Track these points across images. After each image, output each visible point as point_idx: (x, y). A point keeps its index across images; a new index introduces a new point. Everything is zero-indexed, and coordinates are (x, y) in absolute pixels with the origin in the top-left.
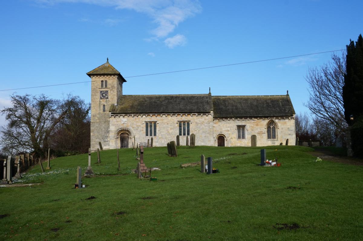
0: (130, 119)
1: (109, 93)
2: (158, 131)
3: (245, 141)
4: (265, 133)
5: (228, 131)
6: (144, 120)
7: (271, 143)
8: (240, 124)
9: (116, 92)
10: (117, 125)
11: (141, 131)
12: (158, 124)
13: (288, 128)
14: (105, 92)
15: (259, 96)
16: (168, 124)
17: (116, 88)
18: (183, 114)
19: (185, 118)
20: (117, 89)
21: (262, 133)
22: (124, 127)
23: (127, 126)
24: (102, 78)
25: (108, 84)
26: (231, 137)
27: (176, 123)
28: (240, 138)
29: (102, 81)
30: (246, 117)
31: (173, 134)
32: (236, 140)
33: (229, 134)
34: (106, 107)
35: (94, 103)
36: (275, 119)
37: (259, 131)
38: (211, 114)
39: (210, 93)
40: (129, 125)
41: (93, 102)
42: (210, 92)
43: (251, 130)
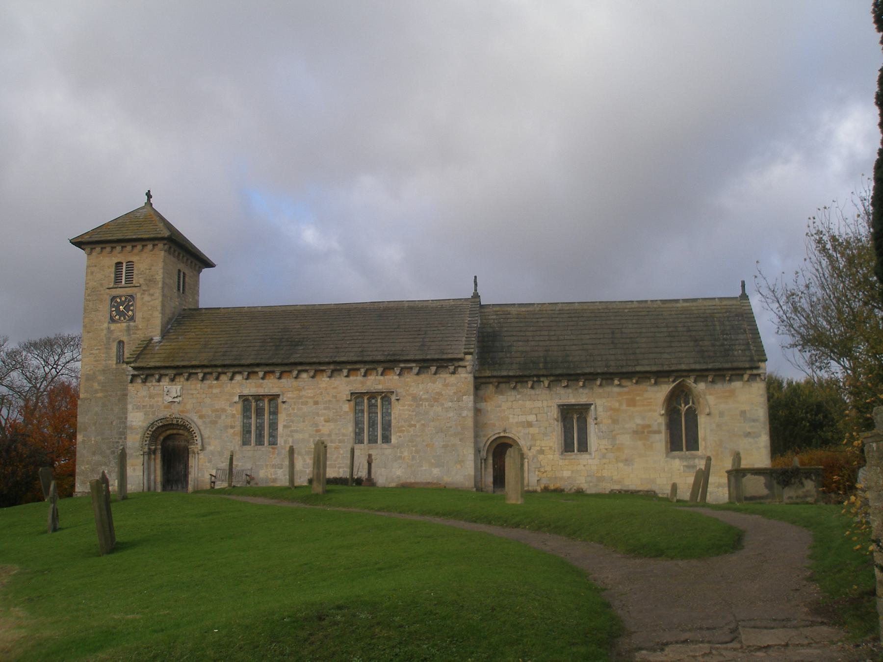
0: (193, 387)
1: (139, 303)
2: (285, 427)
3: (590, 461)
4: (659, 432)
5: (530, 425)
6: (238, 391)
7: (682, 468)
8: (572, 400)
9: (160, 299)
10: (152, 407)
11: (226, 427)
12: (284, 402)
13: (743, 413)
14: (126, 299)
15: (646, 301)
16: (316, 403)
17: (160, 285)
18: (367, 367)
19: (375, 382)
20: (163, 288)
21: (649, 432)
22: (175, 412)
23: (183, 412)
24: (119, 256)
25: (135, 272)
26: (538, 448)
27: (345, 398)
28: (376, 442)
29: (119, 264)
30: (590, 378)
31: (333, 437)
32: (557, 456)
33: (533, 435)
34: (126, 346)
35: (90, 334)
36: (695, 382)
37: (638, 425)
38: (465, 367)
39: (476, 296)
40: (189, 406)
41: (89, 332)
42: (476, 290)
43: (610, 421)
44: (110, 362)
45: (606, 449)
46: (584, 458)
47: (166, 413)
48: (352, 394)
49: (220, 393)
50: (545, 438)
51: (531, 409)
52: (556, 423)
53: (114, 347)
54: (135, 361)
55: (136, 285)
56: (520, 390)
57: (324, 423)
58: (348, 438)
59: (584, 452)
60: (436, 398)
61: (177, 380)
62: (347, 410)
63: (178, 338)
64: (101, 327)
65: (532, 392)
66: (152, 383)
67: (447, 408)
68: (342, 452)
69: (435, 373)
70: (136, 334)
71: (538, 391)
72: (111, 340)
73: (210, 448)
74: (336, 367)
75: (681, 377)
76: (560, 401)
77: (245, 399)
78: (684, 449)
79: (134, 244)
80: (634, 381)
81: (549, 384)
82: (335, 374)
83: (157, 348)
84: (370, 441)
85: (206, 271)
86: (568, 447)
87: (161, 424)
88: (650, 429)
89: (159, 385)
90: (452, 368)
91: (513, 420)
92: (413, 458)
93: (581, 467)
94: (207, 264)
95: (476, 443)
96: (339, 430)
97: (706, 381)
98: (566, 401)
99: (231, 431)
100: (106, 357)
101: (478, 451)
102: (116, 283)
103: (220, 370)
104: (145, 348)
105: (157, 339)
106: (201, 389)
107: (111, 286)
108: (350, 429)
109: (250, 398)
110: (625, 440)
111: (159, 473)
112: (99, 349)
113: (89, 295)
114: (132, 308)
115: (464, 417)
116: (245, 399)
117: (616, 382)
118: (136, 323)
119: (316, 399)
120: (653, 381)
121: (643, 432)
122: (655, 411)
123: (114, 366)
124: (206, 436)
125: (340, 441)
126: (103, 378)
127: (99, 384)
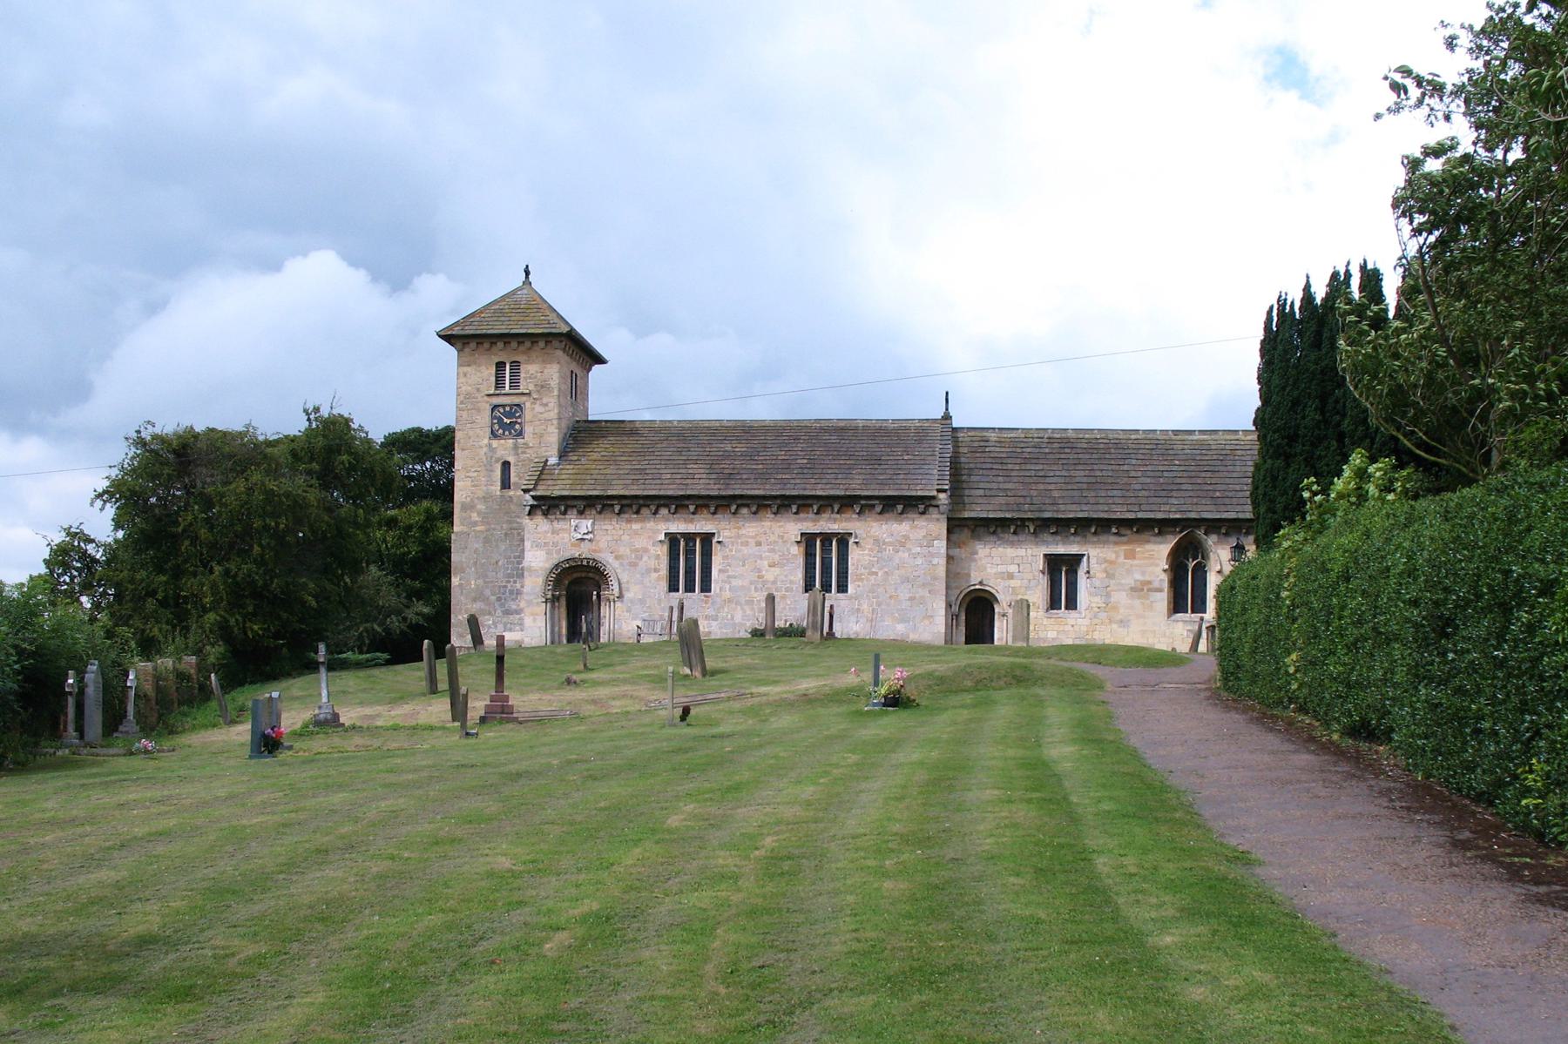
1: (528, 415)
2: (720, 571)
4: (1160, 590)
5: (1011, 576)
8: (1061, 549)
9: (556, 411)
17: (556, 393)
18: (821, 503)
19: (830, 524)
21: (1149, 590)
22: (584, 551)
23: (595, 551)
37: (1136, 581)
39: (947, 417)
40: (603, 544)
42: (947, 409)
44: (493, 488)
47: (573, 552)
48: (802, 534)
51: (1013, 558)
52: (1041, 575)
54: (534, 489)
56: (1001, 535)
60: (902, 543)
61: (587, 512)
62: (796, 552)
65: (1016, 538)
69: (902, 513)
71: (1022, 537)
72: (494, 459)
73: (627, 595)
74: (783, 504)
75: (1189, 527)
77: (673, 539)
79: (521, 340)
80: (1135, 530)
81: (1035, 530)
82: (782, 510)
84: (702, 591)
85: (596, 368)
86: (1054, 604)
88: (1151, 586)
90: (922, 507)
91: (991, 570)
93: (1068, 628)
94: (599, 360)
95: (947, 595)
97: (1219, 534)
99: (654, 575)
101: (949, 605)
102: (497, 388)
103: (641, 502)
104: (542, 473)
105: (553, 460)
107: (492, 392)
108: (799, 576)
109: (679, 536)
110: (1120, 598)
111: (564, 624)
113: (462, 403)
116: (673, 539)
117: (1114, 530)
119: (758, 538)
120: (1156, 530)
122: (1157, 565)
123: (498, 493)
124: (624, 580)
125: (787, 590)
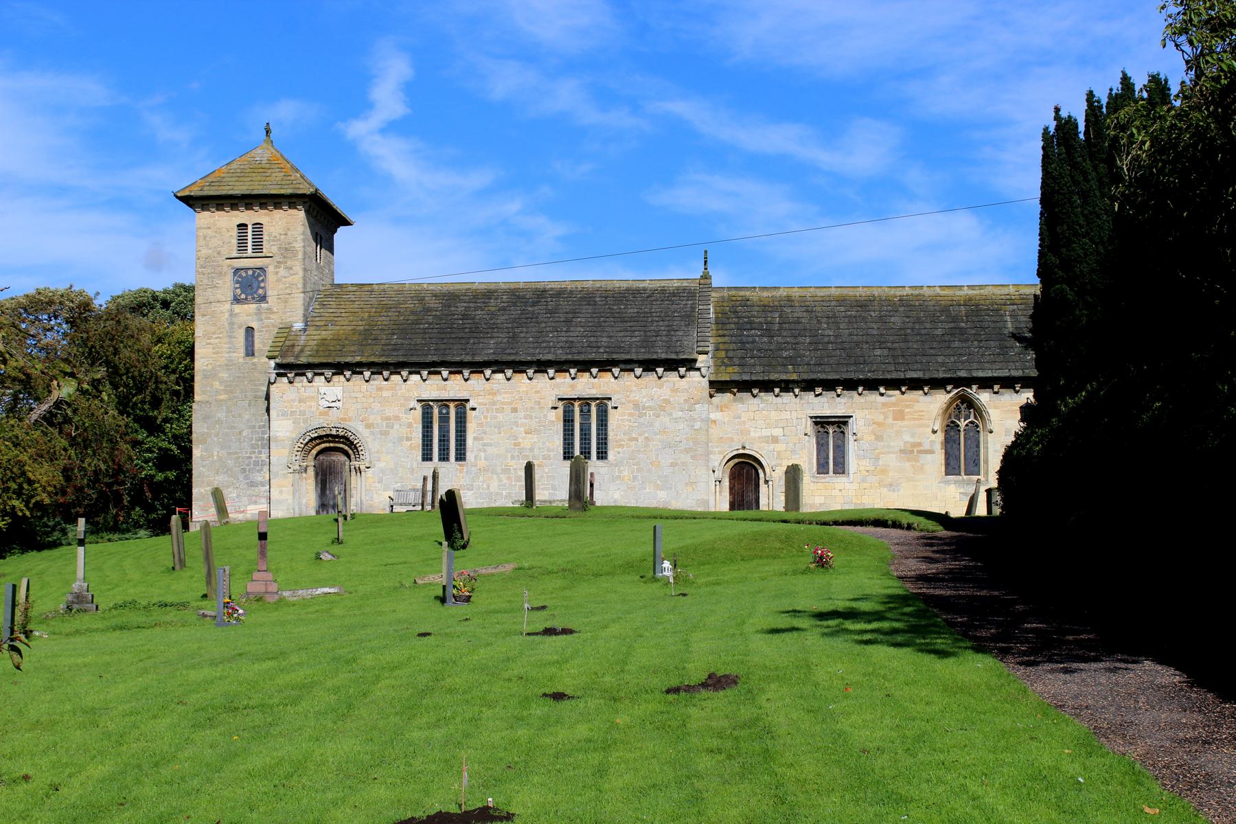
0: (356, 389)
2: (475, 439)
4: (932, 452)
5: (775, 440)
7: (958, 496)
10: (303, 413)
12: (474, 409)
17: (300, 256)
23: (344, 419)
25: (265, 237)
33: (779, 452)
34: (256, 334)
43: (873, 437)
45: (867, 471)
46: (840, 480)
47: (321, 421)
49: (392, 396)
50: (793, 457)
53: (241, 336)
55: (268, 255)
57: (524, 435)
58: (555, 453)
59: (840, 474)
60: (663, 407)
63: (328, 325)
64: (221, 309)
66: (301, 382)
67: (676, 419)
68: (547, 470)
70: (269, 318)
76: (813, 412)
77: (426, 405)
78: (963, 473)
83: (303, 338)
85: (342, 230)
87: (316, 435)
88: (922, 448)
89: (313, 386)
92: (635, 478)
96: (544, 443)
98: (820, 412)
100: (230, 348)
106: (367, 391)
110: (891, 460)
112: (220, 338)
114: (262, 285)
115: (696, 430)
118: (269, 304)
119: (514, 406)
121: (912, 452)
126: (227, 375)
127: (221, 383)
